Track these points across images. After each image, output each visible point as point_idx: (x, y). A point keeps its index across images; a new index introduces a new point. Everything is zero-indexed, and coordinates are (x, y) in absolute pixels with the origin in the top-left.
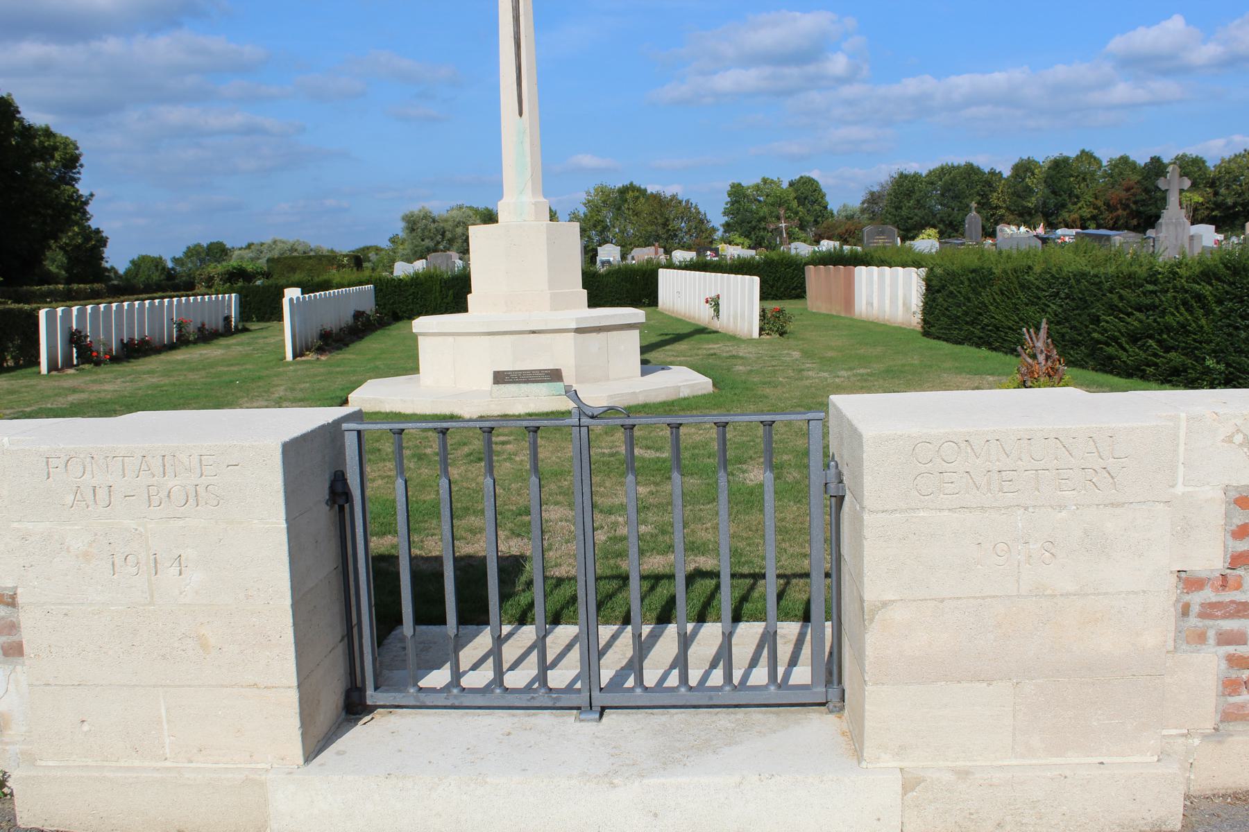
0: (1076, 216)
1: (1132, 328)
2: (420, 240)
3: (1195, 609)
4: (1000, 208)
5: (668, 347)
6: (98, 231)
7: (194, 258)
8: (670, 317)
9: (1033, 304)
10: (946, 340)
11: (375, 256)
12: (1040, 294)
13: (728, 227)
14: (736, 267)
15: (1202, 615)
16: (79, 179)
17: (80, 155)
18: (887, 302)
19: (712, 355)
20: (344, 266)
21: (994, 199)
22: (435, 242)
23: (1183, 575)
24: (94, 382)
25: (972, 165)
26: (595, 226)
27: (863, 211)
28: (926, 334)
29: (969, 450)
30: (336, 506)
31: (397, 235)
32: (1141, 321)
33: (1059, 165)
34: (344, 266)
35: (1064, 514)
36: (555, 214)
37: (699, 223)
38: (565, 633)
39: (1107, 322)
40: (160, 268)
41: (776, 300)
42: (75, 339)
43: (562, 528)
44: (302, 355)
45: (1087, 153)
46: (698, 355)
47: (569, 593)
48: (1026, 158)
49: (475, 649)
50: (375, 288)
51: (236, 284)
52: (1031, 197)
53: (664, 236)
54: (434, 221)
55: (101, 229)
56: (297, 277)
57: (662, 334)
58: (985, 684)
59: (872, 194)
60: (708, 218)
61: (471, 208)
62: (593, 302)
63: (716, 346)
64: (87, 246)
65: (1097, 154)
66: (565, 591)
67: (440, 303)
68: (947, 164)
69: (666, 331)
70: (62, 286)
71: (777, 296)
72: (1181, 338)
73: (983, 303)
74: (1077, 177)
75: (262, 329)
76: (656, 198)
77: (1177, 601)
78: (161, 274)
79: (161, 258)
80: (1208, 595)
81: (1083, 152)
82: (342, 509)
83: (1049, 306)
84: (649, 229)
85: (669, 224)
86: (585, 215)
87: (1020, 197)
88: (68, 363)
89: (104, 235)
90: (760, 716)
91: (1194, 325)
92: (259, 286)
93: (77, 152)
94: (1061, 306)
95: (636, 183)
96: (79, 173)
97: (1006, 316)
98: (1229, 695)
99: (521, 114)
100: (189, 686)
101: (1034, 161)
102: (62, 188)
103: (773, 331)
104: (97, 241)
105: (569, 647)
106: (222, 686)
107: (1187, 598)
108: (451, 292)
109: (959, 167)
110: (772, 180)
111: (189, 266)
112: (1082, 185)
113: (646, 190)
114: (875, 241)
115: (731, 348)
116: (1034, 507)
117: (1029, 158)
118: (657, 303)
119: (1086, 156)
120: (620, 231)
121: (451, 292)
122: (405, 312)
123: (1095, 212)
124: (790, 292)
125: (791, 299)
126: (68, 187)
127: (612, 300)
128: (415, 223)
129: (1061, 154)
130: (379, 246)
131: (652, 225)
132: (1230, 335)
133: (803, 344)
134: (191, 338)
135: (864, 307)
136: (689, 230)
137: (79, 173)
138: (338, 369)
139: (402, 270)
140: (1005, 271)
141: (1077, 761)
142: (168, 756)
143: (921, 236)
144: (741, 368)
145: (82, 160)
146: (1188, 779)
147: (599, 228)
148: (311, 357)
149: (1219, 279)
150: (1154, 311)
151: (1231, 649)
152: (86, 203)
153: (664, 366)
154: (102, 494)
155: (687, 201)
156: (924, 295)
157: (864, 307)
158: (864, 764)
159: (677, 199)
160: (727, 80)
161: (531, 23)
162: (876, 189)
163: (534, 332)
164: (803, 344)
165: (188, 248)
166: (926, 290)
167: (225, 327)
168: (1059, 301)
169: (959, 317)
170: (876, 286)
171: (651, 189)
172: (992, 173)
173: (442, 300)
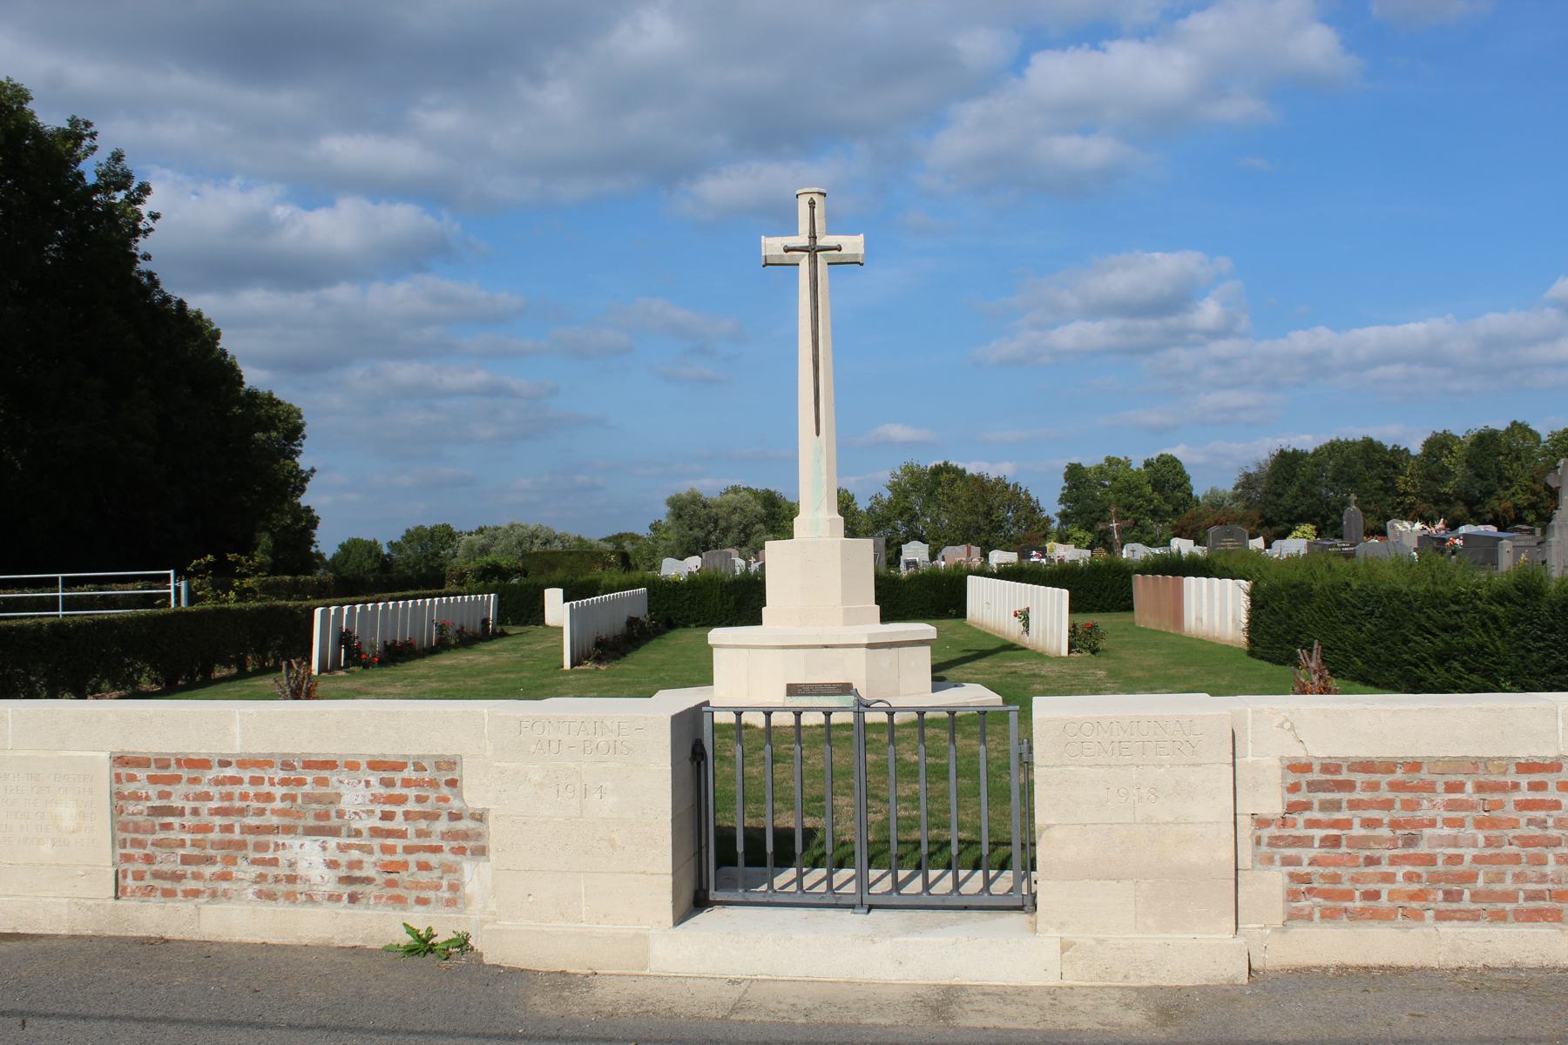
0: (1508, 504)
1: (1439, 649)
2: (687, 529)
3: (1265, 840)
4: (1411, 494)
5: (968, 665)
6: (308, 510)
7: (415, 544)
8: (979, 631)
9: (1350, 623)
10: (1269, 660)
11: (630, 546)
12: (1356, 612)
13: (1064, 517)
14: (1056, 574)
15: (1270, 845)
16: (300, 452)
17: (304, 424)
18: (1217, 617)
19: (1012, 673)
20: (610, 564)
21: (1401, 483)
22: (706, 532)
23: (1255, 817)
24: (373, 684)
25: (1371, 440)
26: (901, 514)
27: (1236, 498)
28: (1251, 654)
29: (1100, 728)
30: (695, 763)
31: (659, 521)
32: (1446, 643)
33: (1486, 440)
34: (610, 564)
35: (1162, 770)
36: (853, 499)
37: (1029, 511)
38: (846, 873)
39: (1417, 643)
40: (373, 554)
41: (1103, 612)
42: (345, 638)
43: (848, 811)
44: (579, 664)
45: (1520, 425)
46: (997, 673)
47: (850, 850)
48: (1441, 432)
49: (781, 879)
50: (648, 590)
51: (491, 582)
52: (1449, 481)
53: (987, 528)
54: (705, 506)
55: (312, 508)
56: (559, 574)
57: (964, 651)
58: (1115, 882)
59: (1248, 476)
60: (1041, 506)
61: (748, 490)
62: (886, 617)
63: (1019, 664)
64: (297, 527)
65: (1533, 427)
66: (848, 849)
67: (720, 610)
68: (1339, 440)
69: (970, 647)
70: (289, 577)
71: (1103, 608)
72: (1481, 660)
73: (1302, 620)
74: (1507, 455)
75: (521, 633)
76: (979, 482)
77: (1253, 834)
78: (375, 561)
79: (375, 542)
80: (1273, 831)
81: (1514, 423)
82: (699, 764)
83: (1365, 626)
84: (969, 518)
85: (993, 514)
86: (890, 502)
87: (1435, 480)
88: (336, 666)
89: (315, 514)
90: (977, 914)
91: (1491, 647)
92: (515, 585)
93: (300, 421)
94: (1376, 625)
95: (953, 463)
96: (301, 445)
97: (1325, 635)
98: (1292, 901)
99: (818, 434)
100: (602, 872)
101: (1451, 435)
102: (282, 463)
103: (1084, 648)
104: (308, 521)
105: (849, 881)
106: (624, 873)
107: (1259, 833)
108: (732, 597)
109: (1354, 443)
110: (1118, 459)
111: (408, 552)
112: (1515, 465)
113: (964, 471)
114: (1222, 544)
115: (1034, 667)
116: (1143, 765)
117: (1445, 431)
118: (966, 614)
119: (1519, 429)
120: (932, 521)
121: (732, 597)
122: (680, 619)
123: (1534, 499)
124: (1119, 603)
125: (1120, 611)
126: (288, 461)
127: (915, 610)
128: (681, 509)
129: (1487, 427)
130: (636, 533)
131: (971, 514)
132: (1522, 657)
133: (1113, 663)
134: (453, 642)
135: (1193, 623)
136: (1018, 521)
137: (301, 445)
138: (622, 680)
139: (675, 569)
140: (1323, 588)
141: (1179, 936)
142: (584, 919)
143: (1294, 534)
144: (1038, 686)
145: (306, 430)
146: (1264, 958)
147: (906, 517)
148: (589, 666)
149: (1510, 601)
150: (1459, 632)
151: (1291, 869)
152: (306, 480)
153: (958, 683)
154: (554, 744)
155: (1016, 486)
156: (1249, 610)
157: (1193, 623)
158: (1037, 934)
159: (1004, 482)
160: (1069, 335)
161: (830, 347)
162: (1253, 470)
163: (826, 647)
164: (1113, 663)
165: (408, 531)
166: (1251, 604)
167: (482, 629)
168: (1374, 620)
169: (1280, 636)
170: (1205, 600)
171: (972, 469)
172: (1396, 451)
173: (722, 606)
